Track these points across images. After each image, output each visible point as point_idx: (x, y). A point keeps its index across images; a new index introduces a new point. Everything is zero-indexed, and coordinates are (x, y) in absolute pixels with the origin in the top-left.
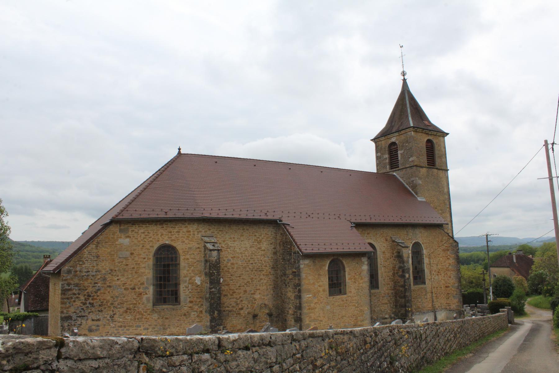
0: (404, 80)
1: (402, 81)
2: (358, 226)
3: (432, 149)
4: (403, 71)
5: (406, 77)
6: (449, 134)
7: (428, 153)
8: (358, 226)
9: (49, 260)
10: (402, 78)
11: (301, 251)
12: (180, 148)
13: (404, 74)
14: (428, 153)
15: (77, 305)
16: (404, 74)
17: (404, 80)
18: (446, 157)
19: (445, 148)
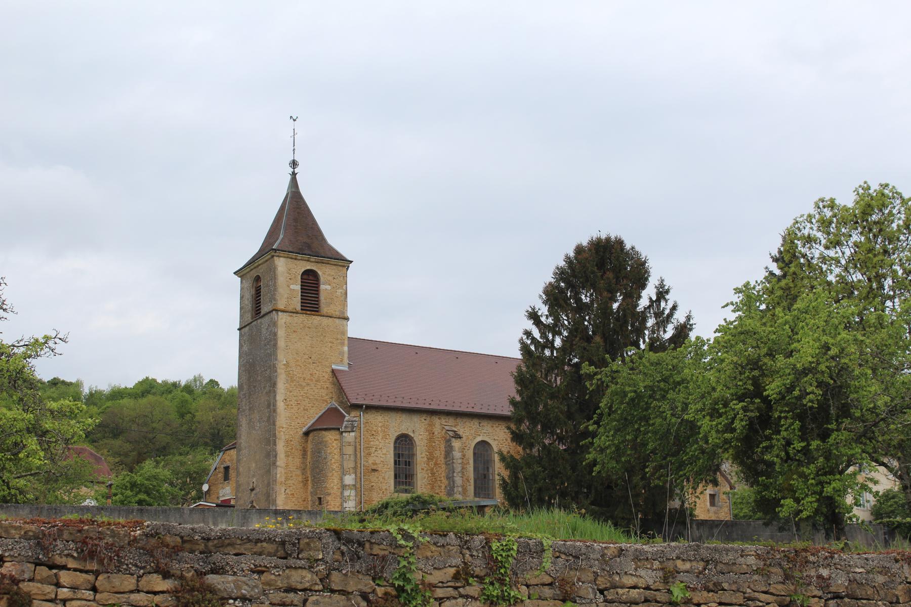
0: (294, 175)
1: (290, 177)
2: (723, 307)
3: (317, 296)
4: (294, 160)
5: (296, 171)
6: (235, 273)
7: (303, 301)
8: (723, 307)
9: (267, 570)
10: (296, 171)
11: (348, 400)
12: (667, 284)
13: (294, 164)
14: (303, 301)
15: (381, 549)
16: (294, 164)
17: (294, 175)
18: (241, 308)
19: (242, 298)
